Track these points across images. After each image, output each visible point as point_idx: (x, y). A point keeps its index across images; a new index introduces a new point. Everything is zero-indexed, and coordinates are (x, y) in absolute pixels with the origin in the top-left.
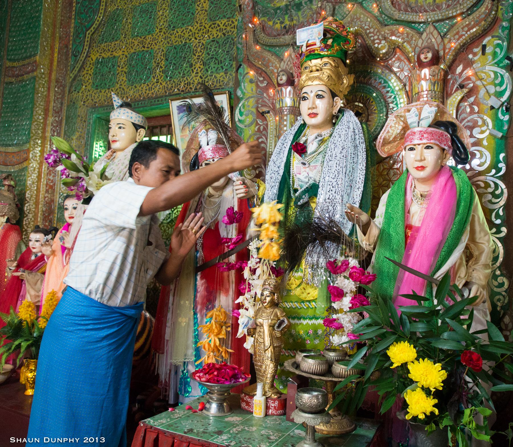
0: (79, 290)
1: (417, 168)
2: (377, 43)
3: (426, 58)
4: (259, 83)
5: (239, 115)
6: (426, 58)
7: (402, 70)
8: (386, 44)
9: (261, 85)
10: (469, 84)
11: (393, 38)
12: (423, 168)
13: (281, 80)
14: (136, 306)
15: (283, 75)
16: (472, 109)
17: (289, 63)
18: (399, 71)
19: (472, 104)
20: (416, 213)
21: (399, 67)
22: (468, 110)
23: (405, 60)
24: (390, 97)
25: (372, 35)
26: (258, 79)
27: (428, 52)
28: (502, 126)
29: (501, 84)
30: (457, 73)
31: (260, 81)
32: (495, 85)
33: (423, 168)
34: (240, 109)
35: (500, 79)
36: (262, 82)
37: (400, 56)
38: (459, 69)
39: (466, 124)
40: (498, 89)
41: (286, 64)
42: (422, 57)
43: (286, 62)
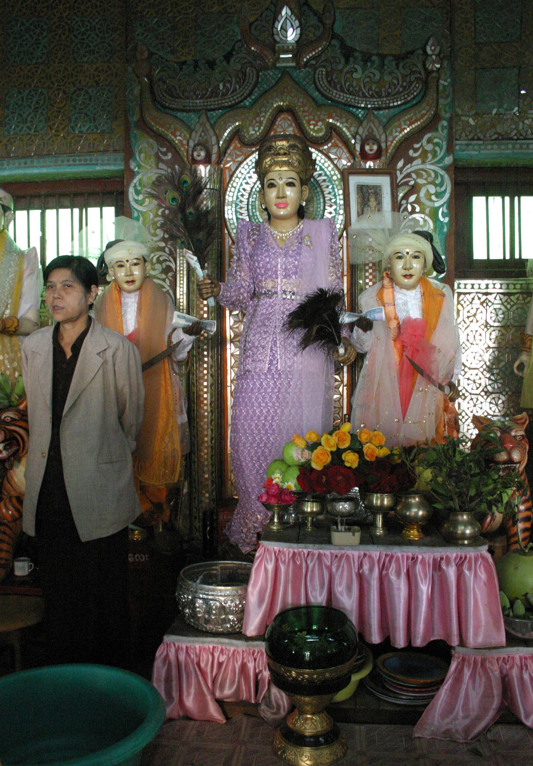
0: (441, 315)
1: (128, 282)
2: (313, 124)
3: (371, 150)
4: (161, 155)
5: (134, 194)
6: (371, 150)
7: (340, 158)
8: (323, 127)
9: (164, 158)
10: (409, 181)
11: (331, 121)
12: (133, 282)
13: (199, 156)
14: (11, 468)
15: (201, 150)
16: (414, 208)
17: (203, 134)
18: (336, 159)
19: (414, 202)
20: (124, 386)
21: (335, 154)
22: (410, 208)
23: (343, 147)
24: (327, 187)
25: (307, 114)
26: (159, 149)
27: (374, 144)
28: (442, 228)
29: (441, 185)
30: (398, 168)
31: (161, 152)
32: (436, 185)
33: (133, 282)
34: (135, 186)
35: (440, 179)
36: (165, 154)
37: (337, 142)
38: (400, 164)
39: (409, 223)
40: (439, 190)
41: (198, 135)
42: (367, 148)
43: (199, 133)
